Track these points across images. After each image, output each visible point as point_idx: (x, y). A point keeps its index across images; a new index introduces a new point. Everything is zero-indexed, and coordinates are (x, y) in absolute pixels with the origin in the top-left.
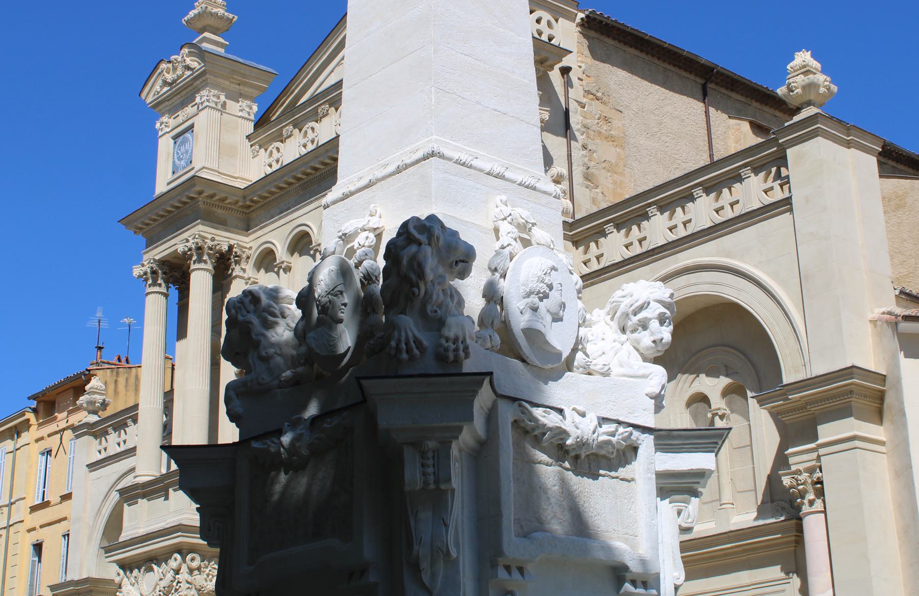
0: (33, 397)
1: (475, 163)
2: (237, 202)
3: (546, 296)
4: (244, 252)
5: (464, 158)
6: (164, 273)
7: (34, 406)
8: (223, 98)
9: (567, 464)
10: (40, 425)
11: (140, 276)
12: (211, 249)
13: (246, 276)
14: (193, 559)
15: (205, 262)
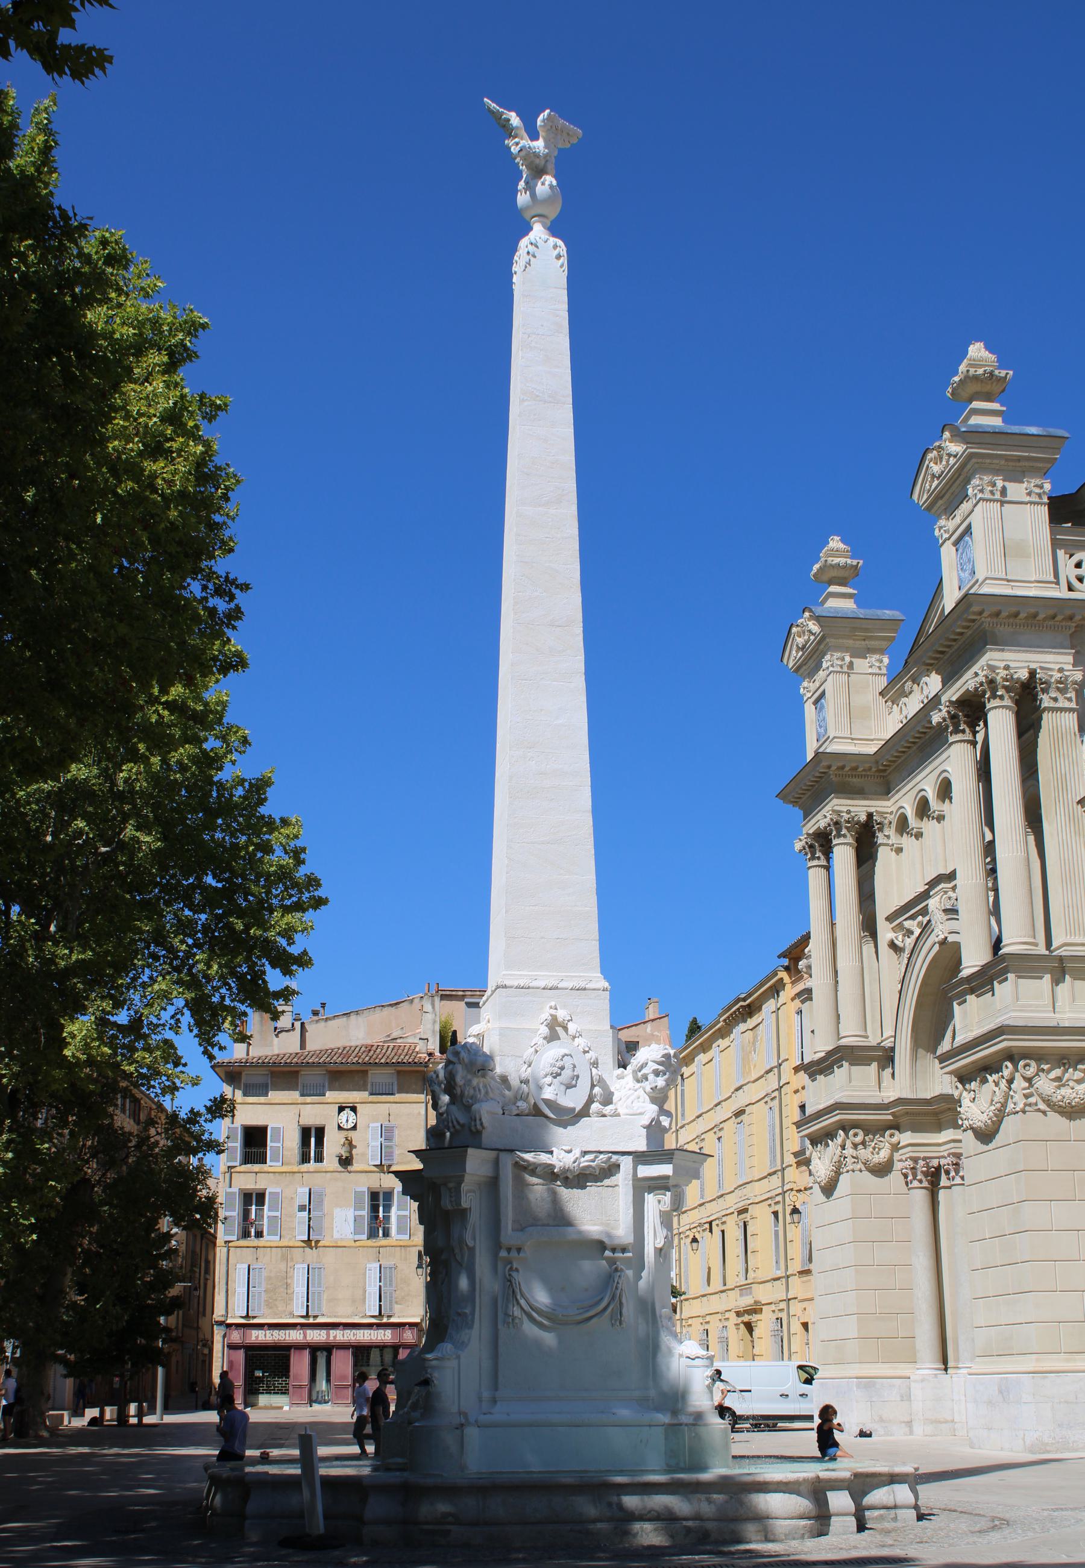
0: (783, 955)
1: (534, 984)
2: (870, 769)
3: (560, 1075)
4: (885, 818)
5: (522, 983)
6: (821, 846)
7: (786, 964)
8: (848, 659)
9: (559, 1183)
10: (793, 983)
11: (800, 851)
12: (848, 822)
13: (890, 842)
14: (855, 1135)
15: (844, 836)
